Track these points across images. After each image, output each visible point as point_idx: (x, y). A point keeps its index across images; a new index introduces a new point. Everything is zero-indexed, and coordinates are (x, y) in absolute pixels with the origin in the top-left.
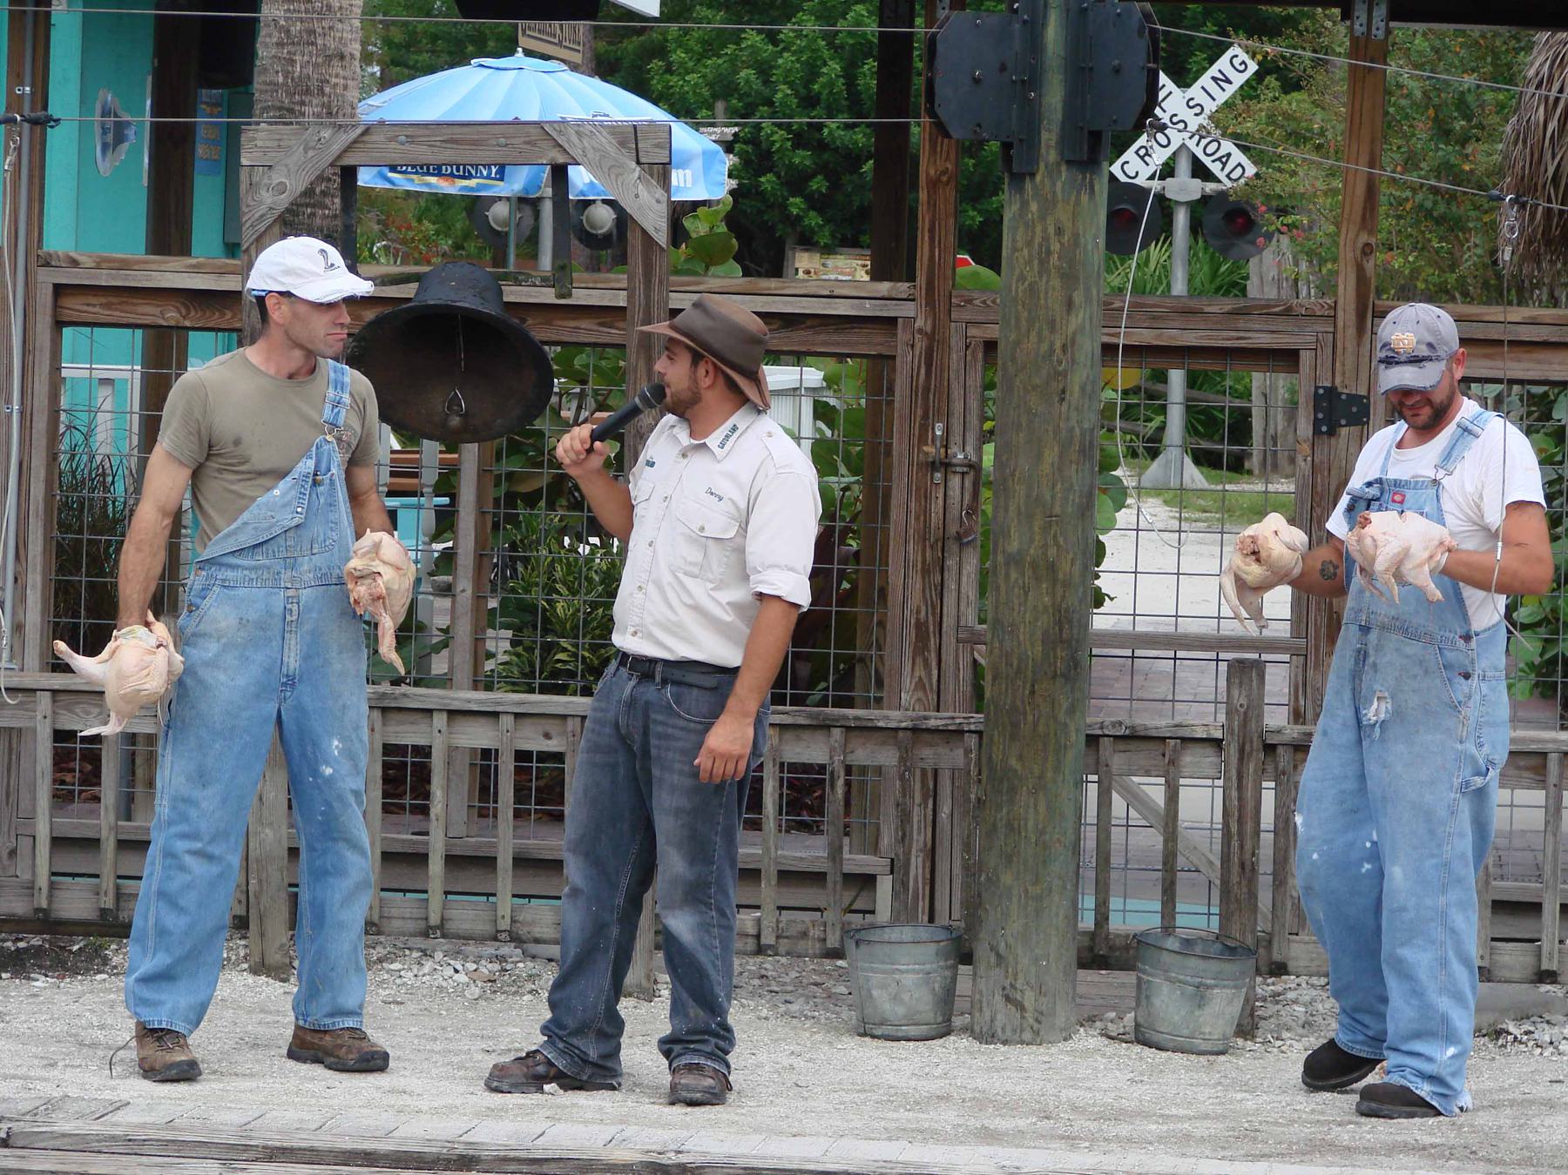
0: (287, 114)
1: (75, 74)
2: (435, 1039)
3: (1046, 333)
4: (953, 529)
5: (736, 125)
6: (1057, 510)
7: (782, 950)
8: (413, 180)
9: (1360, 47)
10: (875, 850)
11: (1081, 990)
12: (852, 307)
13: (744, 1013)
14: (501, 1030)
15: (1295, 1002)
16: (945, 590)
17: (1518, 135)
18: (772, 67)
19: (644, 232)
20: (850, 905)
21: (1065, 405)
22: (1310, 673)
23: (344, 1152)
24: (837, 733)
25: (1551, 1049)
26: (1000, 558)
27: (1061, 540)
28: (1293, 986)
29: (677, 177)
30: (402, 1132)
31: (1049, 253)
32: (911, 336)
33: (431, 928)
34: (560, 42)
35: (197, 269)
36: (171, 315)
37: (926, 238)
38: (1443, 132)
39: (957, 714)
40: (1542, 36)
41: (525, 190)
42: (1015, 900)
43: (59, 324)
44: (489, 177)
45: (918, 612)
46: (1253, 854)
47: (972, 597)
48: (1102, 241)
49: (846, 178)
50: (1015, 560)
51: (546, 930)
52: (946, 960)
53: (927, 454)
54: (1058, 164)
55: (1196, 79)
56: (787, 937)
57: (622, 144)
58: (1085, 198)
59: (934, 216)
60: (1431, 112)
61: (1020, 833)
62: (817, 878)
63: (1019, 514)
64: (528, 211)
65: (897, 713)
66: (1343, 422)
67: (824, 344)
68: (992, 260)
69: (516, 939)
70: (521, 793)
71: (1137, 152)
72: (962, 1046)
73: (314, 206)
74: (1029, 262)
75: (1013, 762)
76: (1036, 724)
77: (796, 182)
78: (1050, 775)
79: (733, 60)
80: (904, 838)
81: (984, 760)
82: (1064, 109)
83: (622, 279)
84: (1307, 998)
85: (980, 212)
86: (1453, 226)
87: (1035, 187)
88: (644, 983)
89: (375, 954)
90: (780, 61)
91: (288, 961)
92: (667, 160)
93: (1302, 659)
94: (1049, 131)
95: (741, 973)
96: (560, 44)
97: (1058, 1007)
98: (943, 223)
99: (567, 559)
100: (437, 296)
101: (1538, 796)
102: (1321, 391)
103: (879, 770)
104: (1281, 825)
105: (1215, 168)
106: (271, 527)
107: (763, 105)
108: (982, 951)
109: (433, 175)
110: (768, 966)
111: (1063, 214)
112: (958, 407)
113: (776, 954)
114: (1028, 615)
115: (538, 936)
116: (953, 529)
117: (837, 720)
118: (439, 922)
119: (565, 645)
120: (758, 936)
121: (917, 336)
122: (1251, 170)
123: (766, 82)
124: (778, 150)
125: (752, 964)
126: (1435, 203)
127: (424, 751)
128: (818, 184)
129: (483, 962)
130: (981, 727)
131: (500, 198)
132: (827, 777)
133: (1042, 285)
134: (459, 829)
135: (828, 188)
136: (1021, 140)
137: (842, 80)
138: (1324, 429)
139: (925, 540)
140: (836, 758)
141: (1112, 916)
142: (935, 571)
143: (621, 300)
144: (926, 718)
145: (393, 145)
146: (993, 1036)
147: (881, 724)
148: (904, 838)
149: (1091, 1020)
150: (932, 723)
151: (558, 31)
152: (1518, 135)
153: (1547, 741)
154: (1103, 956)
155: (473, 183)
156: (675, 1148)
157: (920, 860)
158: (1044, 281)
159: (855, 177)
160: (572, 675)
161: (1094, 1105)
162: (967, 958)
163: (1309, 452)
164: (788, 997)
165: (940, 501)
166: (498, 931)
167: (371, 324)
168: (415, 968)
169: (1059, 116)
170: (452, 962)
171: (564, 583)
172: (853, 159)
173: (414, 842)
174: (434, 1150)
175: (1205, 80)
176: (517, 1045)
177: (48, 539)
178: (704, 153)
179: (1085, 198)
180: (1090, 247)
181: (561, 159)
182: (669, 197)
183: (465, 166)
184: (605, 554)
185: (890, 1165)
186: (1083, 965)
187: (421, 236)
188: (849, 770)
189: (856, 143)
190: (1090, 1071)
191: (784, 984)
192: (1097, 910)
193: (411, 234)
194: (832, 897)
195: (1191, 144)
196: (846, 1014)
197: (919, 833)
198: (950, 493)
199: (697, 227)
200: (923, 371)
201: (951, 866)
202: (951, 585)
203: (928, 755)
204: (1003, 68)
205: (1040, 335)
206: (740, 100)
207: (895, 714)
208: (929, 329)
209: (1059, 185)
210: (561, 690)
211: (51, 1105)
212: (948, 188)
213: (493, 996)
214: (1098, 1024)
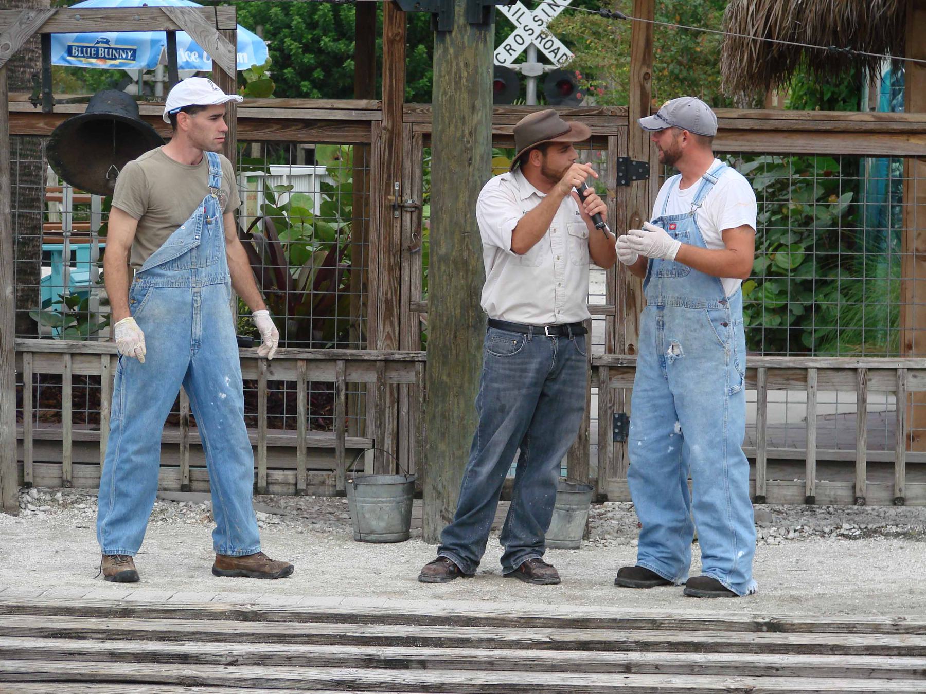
3: (460, 125)
4: (406, 244)
6: (468, 229)
7: (310, 492)
8: (81, 61)
10: (363, 435)
12: (345, 115)
13: (288, 530)
15: (612, 518)
16: (402, 281)
17: (732, 16)
19: (221, 68)
20: (350, 467)
21: (471, 168)
22: (617, 326)
23: (54, 608)
24: (340, 364)
25: (763, 542)
26: (435, 258)
27: (471, 247)
28: (610, 509)
30: (89, 596)
31: (460, 78)
32: (379, 132)
37: (388, 73)
39: (410, 351)
41: (148, 65)
42: (447, 459)
44: (126, 58)
45: (386, 294)
46: (587, 431)
47: (418, 285)
49: (335, 70)
51: (171, 483)
52: (408, 495)
53: (390, 201)
54: (465, 26)
56: (312, 485)
58: (481, 46)
59: (392, 59)
60: (678, 18)
61: (449, 419)
62: (330, 451)
63: (446, 231)
65: (376, 351)
66: (634, 178)
67: (329, 136)
71: (505, 48)
72: (417, 546)
73: (24, 67)
74: (449, 84)
75: (444, 378)
76: (457, 355)
78: (466, 385)
80: (380, 425)
81: (427, 377)
84: (619, 516)
85: (412, 89)
87: (452, 40)
89: (69, 499)
91: (18, 504)
93: (612, 317)
94: (459, 6)
95: (286, 508)
100: (99, 110)
102: (621, 160)
103: (365, 385)
104: (602, 414)
105: (550, 56)
108: (427, 490)
109: (93, 58)
110: (302, 503)
111: (468, 55)
112: (408, 172)
113: (307, 495)
114: (452, 291)
115: (166, 486)
116: (406, 244)
117: (341, 356)
120: (296, 484)
121: (383, 131)
123: (287, 15)
124: (294, 54)
125: (293, 502)
126: (681, 71)
127: (96, 379)
128: (318, 74)
130: (425, 359)
132: (335, 392)
133: (457, 96)
135: (324, 76)
136: (443, 12)
137: (331, 13)
138: (623, 182)
139: (390, 251)
140: (340, 379)
142: (396, 270)
144: (393, 354)
145: (73, 20)
146: (435, 540)
147: (366, 358)
148: (380, 425)
150: (396, 357)
152: (732, 16)
153: (758, 361)
155: (117, 62)
157: (390, 439)
158: (458, 93)
159: (340, 70)
162: (419, 495)
163: (614, 196)
164: (314, 520)
165: (399, 228)
167: (61, 126)
172: (339, 59)
173: (91, 435)
174: (107, 606)
179: (481, 46)
180: (484, 75)
181: (172, 28)
188: (347, 384)
189: (340, 49)
191: (312, 513)
194: (339, 463)
195: (536, 43)
196: (348, 529)
197: (389, 424)
198: (404, 223)
200: (387, 153)
201: (408, 443)
202: (406, 277)
203: (395, 376)
205: (456, 126)
207: (374, 352)
208: (390, 127)
209: (466, 37)
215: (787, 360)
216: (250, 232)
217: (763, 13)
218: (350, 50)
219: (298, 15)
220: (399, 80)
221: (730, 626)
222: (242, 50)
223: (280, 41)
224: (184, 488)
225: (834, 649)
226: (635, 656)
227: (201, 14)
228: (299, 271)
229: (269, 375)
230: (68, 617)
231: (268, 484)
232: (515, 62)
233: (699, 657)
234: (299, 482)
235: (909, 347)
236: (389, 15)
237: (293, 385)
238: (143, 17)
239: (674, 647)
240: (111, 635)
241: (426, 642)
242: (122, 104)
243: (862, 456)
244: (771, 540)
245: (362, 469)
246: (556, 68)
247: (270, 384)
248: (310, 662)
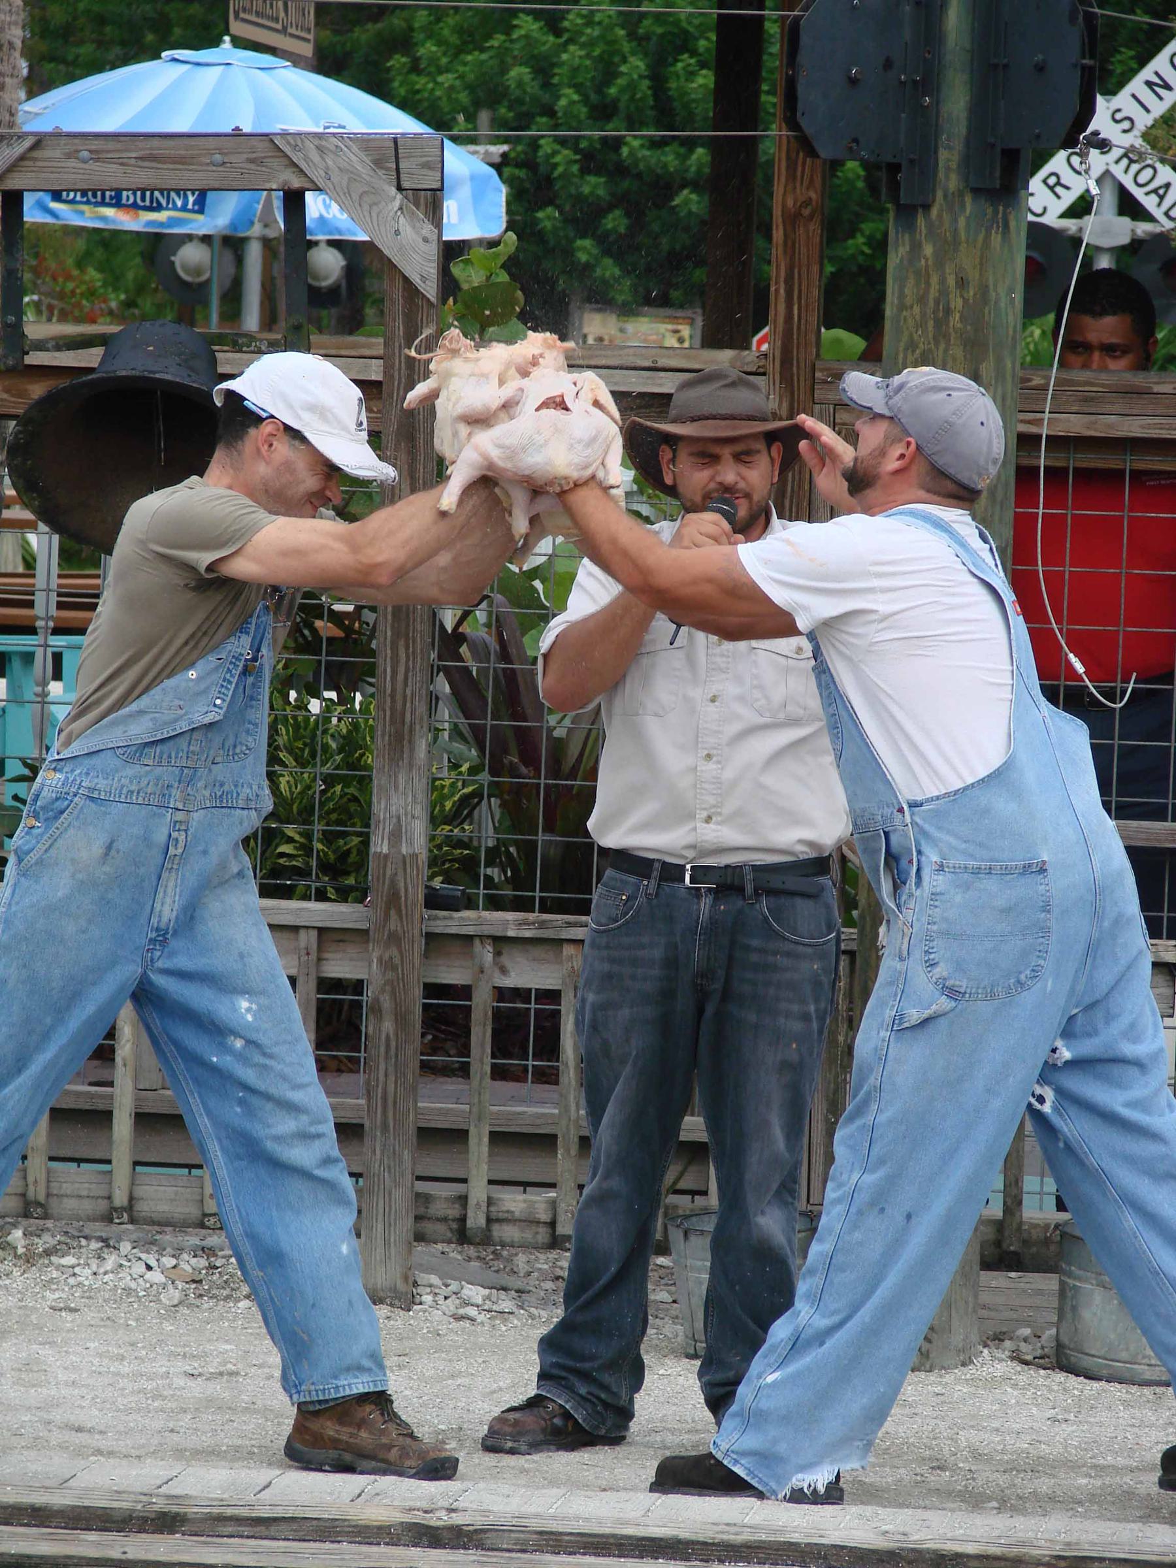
2: (122, 1358)
5: (506, 140)
8: (82, 213)
11: (984, 1298)
14: (209, 1347)
18: (553, 65)
19: (406, 279)
29: (450, 208)
31: (948, 311)
33: (116, 1209)
34: (285, 29)
37: (782, 291)
41: (233, 225)
44: (184, 208)
48: (1018, 296)
54: (961, 194)
55: (1121, 85)
57: (378, 163)
64: (229, 256)
74: (922, 324)
79: (502, 52)
82: (969, 119)
87: (930, 227)
88: (401, 1286)
89: (41, 1244)
90: (565, 57)
92: (437, 185)
94: (949, 148)
95: (529, 1274)
96: (284, 31)
97: (955, 1323)
98: (804, 269)
99: (295, 718)
100: (129, 365)
105: (1149, 203)
106: (176, 720)
107: (542, 115)
109: (109, 205)
111: (967, 259)
118: (125, 1203)
119: (290, 834)
120: (552, 1224)
123: (546, 85)
124: (562, 176)
128: (615, 221)
129: (185, 1256)
130: (853, 946)
131: (190, 237)
134: (152, 1078)
136: (912, 161)
141: (1026, 1199)
145: (72, 163)
149: (998, 1338)
151: (282, 14)
154: (1015, 1253)
155: (162, 216)
156: (446, 1504)
158: (942, 346)
160: (303, 873)
161: (1003, 1452)
166: (205, 1215)
168: (94, 1263)
169: (963, 130)
170: (143, 1256)
171: (290, 751)
174: (125, 1505)
175: (1137, 85)
176: (230, 1366)
178: (473, 178)
179: (996, 239)
180: (1002, 305)
181: (296, 183)
182: (440, 234)
183: (143, 191)
184: (345, 712)
185: (733, 1529)
186: (987, 1265)
187: (84, 288)
189: (665, 166)
190: (996, 1407)
192: (1005, 1192)
193: (70, 286)
195: (1118, 171)
204: (888, 64)
206: (510, 108)
209: (962, 222)
212: (812, 227)
213: (198, 1302)
214: (1008, 1344)
216: (460, 630)
218: (687, 170)
219: (570, 87)
220: (807, 305)
223: (529, 145)
227: (362, 155)
228: (567, 722)
229: (497, 974)
230: (34, 1530)
231: (489, 1220)
234: (561, 1218)
236: (788, 158)
237: (553, 996)
238: (233, 159)
242: (179, 355)
245: (704, 1189)
246: (1158, 229)
247: (501, 993)
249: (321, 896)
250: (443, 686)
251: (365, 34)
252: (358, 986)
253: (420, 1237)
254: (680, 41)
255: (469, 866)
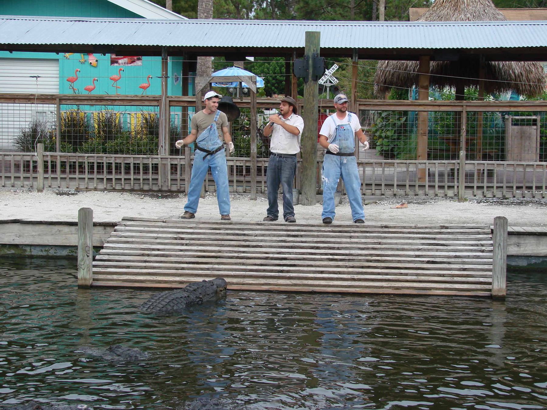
0: (201, 75)
1: (171, 70)
9: (354, 63)
35: (189, 98)
36: (186, 105)
38: (365, 75)
40: (380, 61)
43: (170, 106)
48: (318, 91)
50: (306, 137)
64: (235, 90)
68: (302, 95)
69: (236, 192)
70: (237, 172)
77: (273, 85)
83: (250, 98)
86: (367, 89)
101: (381, 169)
105: (333, 82)
108: (303, 193)
122: (338, 82)
128: (276, 85)
143: (250, 101)
149: (318, 202)
162: (301, 194)
172: (281, 81)
175: (331, 69)
177: (169, 136)
186: (317, 194)
199: (260, 91)
210: (242, 157)
211: (172, 217)
215: (390, 161)
217: (384, 75)
221: (375, 227)
222: (258, 82)
224: (244, 192)
225: (400, 233)
226: (352, 234)
232: (324, 83)
233: (368, 234)
235: (419, 156)
239: (362, 232)
240: (227, 229)
241: (302, 231)
243: (407, 183)
244: (385, 204)
248: (274, 236)
249: (246, 157)
250: (258, 134)
251: (249, 66)
252: (250, 166)
253: (257, 193)
254: (283, 66)
255: (261, 153)
